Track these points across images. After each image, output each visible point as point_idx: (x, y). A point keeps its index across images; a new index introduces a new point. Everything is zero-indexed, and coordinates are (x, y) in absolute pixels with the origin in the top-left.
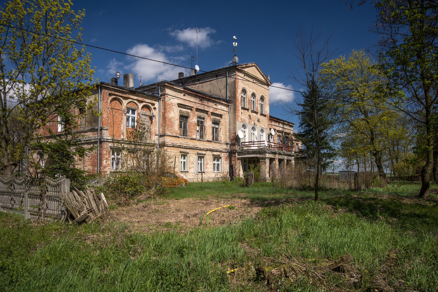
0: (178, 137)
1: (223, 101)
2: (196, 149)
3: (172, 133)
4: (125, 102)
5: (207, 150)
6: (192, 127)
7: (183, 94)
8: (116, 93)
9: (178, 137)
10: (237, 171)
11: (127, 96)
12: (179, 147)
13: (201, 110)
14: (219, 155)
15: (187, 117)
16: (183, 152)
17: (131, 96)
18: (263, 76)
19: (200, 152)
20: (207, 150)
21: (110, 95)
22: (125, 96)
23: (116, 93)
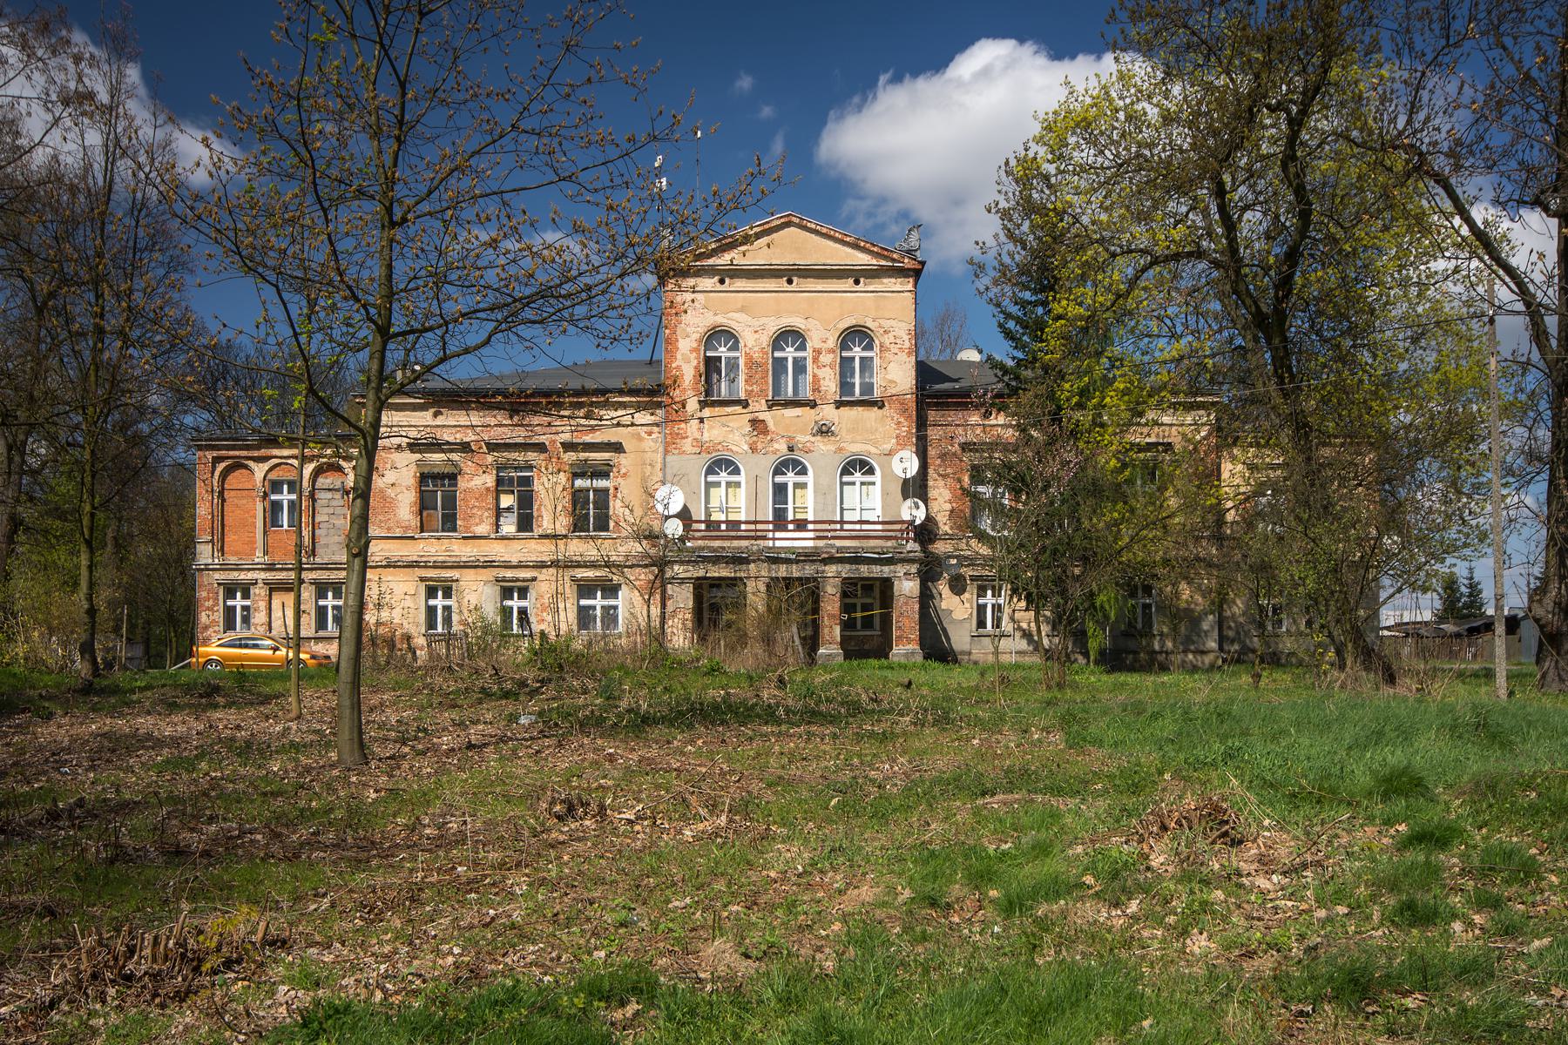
0: (412, 538)
1: (621, 392)
2: (489, 565)
3: (389, 529)
4: (260, 470)
5: (541, 565)
6: (473, 502)
7: (432, 411)
8: (231, 453)
9: (412, 538)
10: (826, 630)
11: (263, 452)
12: (489, 565)
13: (516, 444)
14: (76, 584)
15: (452, 477)
16: (504, 580)
17: (276, 452)
18: (855, 246)
19: (509, 574)
20: (541, 565)
21: (217, 460)
22: (256, 454)
23: (231, 453)
